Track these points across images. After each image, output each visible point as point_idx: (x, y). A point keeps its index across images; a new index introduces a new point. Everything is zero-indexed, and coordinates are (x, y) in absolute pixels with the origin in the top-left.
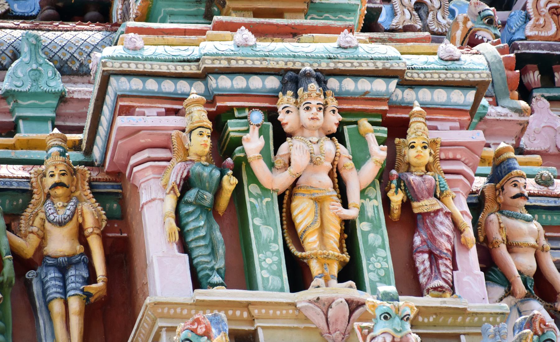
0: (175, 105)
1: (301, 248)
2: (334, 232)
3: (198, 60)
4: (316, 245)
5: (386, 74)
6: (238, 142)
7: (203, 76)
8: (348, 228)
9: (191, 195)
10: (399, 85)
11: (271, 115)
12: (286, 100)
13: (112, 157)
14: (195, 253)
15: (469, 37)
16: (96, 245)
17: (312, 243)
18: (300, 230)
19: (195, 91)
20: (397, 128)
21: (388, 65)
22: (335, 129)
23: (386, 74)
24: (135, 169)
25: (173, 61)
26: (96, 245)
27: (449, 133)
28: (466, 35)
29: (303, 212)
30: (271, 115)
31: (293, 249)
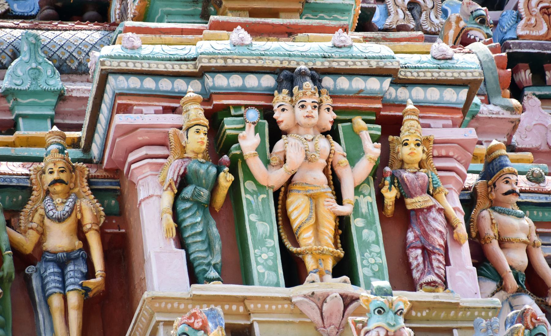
0: (172, 103)
1: (296, 244)
2: (329, 228)
3: (194, 59)
4: (311, 241)
5: (379, 73)
6: (234, 140)
7: (200, 75)
8: (343, 224)
9: (188, 191)
10: (392, 84)
11: (267, 113)
12: (281, 98)
13: (110, 155)
14: (192, 249)
15: (462, 37)
16: (94, 241)
17: (307, 238)
18: (295, 226)
19: (192, 89)
20: (390, 126)
21: (381, 64)
22: (329, 127)
23: (379, 73)
24: (133, 166)
25: (170, 60)
26: (94, 241)
27: (441, 131)
28: (459, 35)
29: (298, 208)
30: (267, 113)
31: (288, 245)
